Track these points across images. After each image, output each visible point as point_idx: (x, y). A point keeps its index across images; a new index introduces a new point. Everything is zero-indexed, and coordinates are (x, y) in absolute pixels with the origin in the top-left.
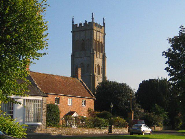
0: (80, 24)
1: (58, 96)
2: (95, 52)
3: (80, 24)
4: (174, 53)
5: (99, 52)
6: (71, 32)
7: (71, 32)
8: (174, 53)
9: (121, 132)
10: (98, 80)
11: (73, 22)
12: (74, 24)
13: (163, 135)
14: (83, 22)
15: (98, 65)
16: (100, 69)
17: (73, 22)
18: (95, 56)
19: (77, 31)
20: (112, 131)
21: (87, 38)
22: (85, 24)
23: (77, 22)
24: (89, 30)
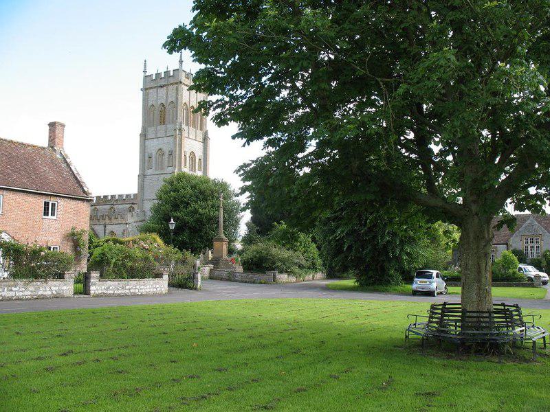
0: (158, 74)
1: (171, 139)
2: (184, 126)
3: (158, 74)
4: (337, 157)
5: (194, 126)
6: (142, 90)
7: (142, 90)
8: (337, 157)
9: (131, 291)
10: (128, 228)
11: (145, 72)
12: (147, 74)
13: (382, 323)
14: (162, 71)
15: (192, 153)
16: (197, 160)
17: (145, 72)
18: (185, 134)
19: (151, 88)
20: (92, 288)
21: (169, 100)
22: (167, 73)
23: (152, 71)
24: (172, 84)
